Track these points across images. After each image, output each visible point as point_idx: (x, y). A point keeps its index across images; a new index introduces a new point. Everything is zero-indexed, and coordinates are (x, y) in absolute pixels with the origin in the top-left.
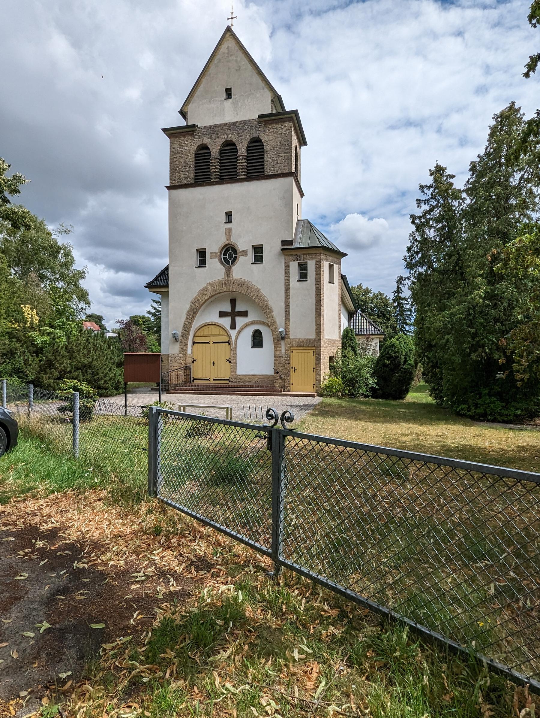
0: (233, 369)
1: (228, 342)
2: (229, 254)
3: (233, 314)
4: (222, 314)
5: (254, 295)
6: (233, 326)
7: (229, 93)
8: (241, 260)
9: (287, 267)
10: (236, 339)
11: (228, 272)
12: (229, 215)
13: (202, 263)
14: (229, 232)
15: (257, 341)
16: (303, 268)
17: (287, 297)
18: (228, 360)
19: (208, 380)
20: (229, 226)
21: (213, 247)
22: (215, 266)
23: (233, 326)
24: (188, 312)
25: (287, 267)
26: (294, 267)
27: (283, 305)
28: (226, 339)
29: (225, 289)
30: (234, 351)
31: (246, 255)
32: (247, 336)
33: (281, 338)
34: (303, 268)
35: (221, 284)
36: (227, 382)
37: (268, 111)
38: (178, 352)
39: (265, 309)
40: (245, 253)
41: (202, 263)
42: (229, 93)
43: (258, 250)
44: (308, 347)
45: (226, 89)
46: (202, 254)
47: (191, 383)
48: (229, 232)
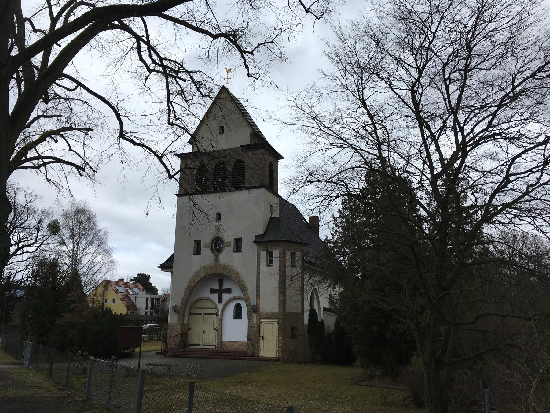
0: (220, 336)
1: (217, 314)
2: (217, 244)
3: (221, 291)
4: (213, 291)
5: (234, 277)
6: (220, 301)
7: (222, 128)
8: (226, 249)
9: (259, 255)
10: (223, 311)
11: (217, 258)
12: (219, 215)
13: (198, 251)
14: (218, 228)
15: (238, 314)
16: (270, 255)
17: (258, 279)
18: (215, 329)
19: (200, 345)
20: (218, 223)
21: (206, 239)
22: (206, 252)
23: (220, 301)
24: (186, 289)
25: (259, 255)
26: (264, 254)
27: (255, 284)
28: (214, 311)
29: (213, 272)
30: (221, 321)
31: (230, 246)
32: (230, 310)
33: (254, 310)
34: (270, 255)
35: (211, 267)
36: (214, 347)
37: (248, 142)
38: (176, 322)
39: (243, 288)
40: (228, 244)
41: (198, 251)
42: (222, 128)
43: (238, 241)
44: (273, 319)
45: (221, 127)
46: (198, 243)
47: (185, 348)
48: (218, 228)
